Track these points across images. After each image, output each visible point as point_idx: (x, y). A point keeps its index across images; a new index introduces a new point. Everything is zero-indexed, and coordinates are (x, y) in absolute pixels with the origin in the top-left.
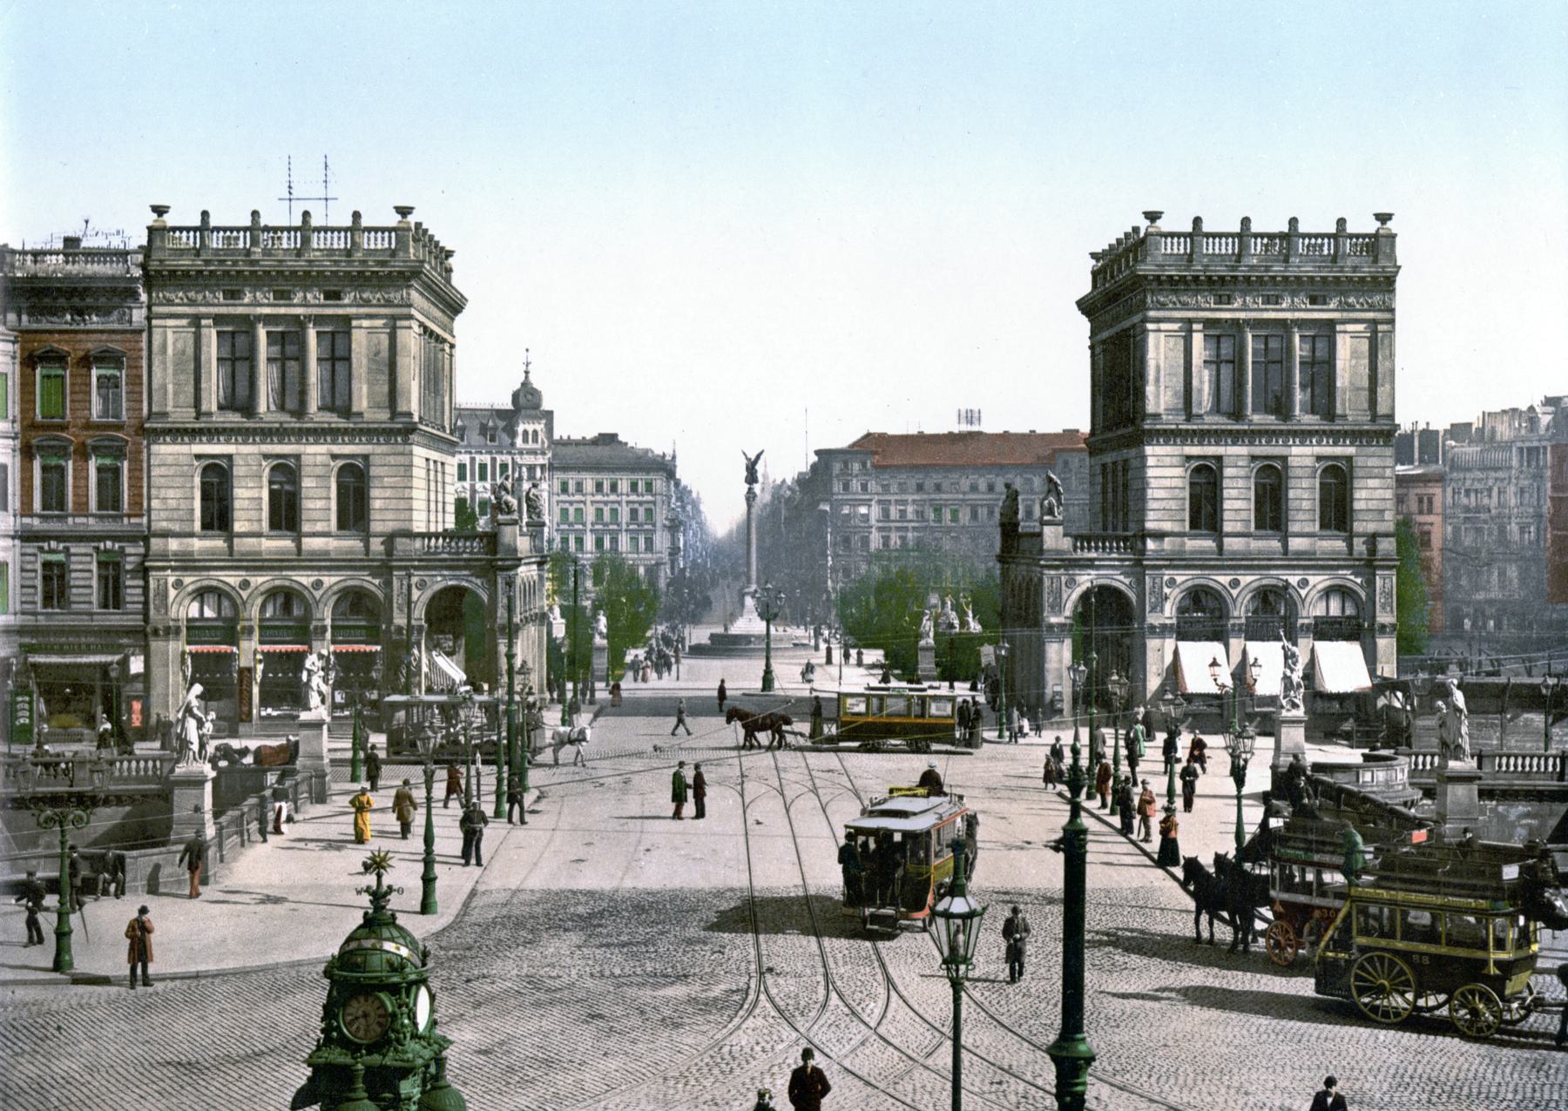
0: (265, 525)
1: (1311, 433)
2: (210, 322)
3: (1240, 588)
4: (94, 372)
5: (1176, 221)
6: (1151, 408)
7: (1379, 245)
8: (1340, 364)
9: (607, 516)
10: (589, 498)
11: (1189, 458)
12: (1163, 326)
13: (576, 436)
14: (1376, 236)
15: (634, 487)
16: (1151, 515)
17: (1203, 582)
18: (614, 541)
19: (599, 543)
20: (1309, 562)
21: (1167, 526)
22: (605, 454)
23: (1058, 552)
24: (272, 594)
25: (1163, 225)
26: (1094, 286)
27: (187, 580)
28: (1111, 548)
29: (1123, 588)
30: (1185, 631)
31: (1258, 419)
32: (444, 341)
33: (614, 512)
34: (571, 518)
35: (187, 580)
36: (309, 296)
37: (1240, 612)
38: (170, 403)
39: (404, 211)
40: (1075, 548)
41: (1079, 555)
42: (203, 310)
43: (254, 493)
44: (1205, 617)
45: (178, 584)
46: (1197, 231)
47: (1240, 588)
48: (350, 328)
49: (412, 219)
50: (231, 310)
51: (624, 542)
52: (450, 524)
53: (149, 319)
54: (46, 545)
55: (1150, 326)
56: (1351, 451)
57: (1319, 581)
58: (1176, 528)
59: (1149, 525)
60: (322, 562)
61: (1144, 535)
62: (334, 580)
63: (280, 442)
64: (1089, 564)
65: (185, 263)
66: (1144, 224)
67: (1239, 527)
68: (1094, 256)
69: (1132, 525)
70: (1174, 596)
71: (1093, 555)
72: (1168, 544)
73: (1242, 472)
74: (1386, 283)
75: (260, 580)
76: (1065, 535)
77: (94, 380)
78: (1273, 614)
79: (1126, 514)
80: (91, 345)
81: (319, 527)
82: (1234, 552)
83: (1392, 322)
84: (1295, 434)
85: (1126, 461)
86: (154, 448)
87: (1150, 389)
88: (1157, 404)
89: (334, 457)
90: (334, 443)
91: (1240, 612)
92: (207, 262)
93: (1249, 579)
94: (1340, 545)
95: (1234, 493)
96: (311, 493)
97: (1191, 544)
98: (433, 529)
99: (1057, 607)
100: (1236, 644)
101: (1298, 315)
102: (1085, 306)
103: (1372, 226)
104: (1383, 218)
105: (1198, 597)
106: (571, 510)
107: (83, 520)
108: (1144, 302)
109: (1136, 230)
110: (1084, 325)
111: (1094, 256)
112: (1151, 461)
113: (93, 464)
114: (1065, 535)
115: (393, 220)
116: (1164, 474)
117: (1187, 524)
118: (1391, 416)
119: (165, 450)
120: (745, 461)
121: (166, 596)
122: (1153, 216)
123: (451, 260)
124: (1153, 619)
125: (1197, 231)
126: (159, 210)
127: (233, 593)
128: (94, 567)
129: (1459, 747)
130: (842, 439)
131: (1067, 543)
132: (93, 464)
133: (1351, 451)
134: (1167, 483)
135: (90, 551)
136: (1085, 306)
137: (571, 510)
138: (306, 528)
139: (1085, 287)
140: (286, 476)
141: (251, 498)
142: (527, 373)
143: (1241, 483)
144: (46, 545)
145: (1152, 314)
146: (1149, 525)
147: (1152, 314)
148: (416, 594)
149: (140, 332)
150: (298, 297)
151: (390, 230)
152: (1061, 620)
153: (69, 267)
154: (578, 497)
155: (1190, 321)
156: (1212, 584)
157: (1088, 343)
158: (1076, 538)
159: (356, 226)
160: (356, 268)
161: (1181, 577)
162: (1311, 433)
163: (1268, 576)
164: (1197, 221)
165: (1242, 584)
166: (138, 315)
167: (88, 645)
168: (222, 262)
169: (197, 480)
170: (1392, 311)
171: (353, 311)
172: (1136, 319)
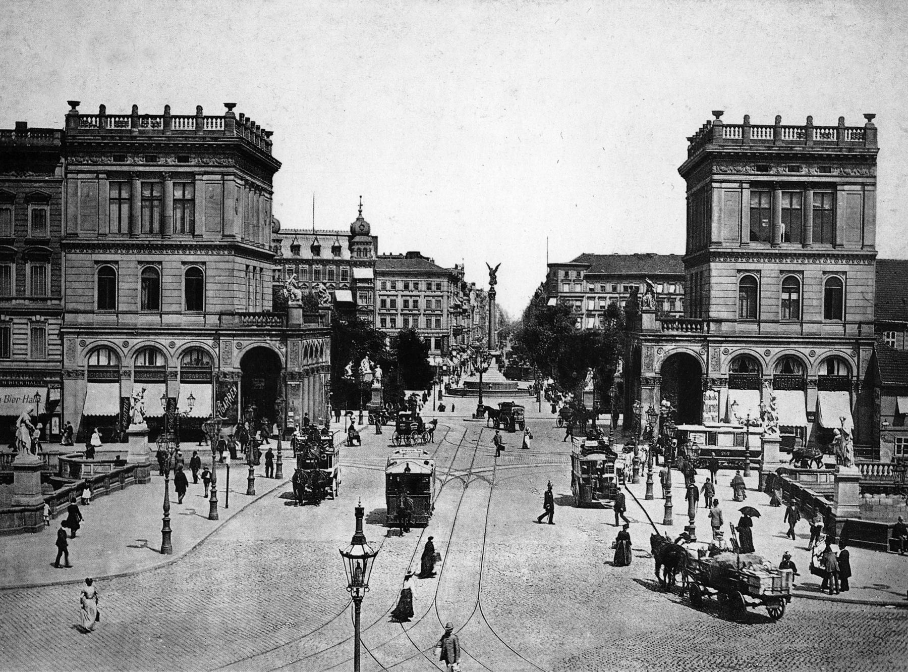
0: (183, 306)
1: (820, 256)
2: (104, 176)
3: (769, 358)
4: (30, 208)
5: (732, 117)
6: (714, 238)
7: (868, 133)
8: (839, 212)
9: (434, 306)
10: (400, 293)
11: (739, 271)
12: (724, 185)
13: (396, 253)
14: (865, 129)
15: (406, 287)
16: (713, 308)
17: (747, 351)
18: (415, 321)
19: (406, 322)
20: (814, 340)
21: (724, 315)
22: (415, 265)
23: (651, 331)
24: (188, 351)
25: (725, 120)
26: (689, 157)
27: (88, 341)
28: (687, 328)
29: (847, 357)
30: (733, 383)
31: (817, 248)
32: (265, 190)
33: (416, 302)
34: (411, 307)
35: (244, 343)
36: (169, 160)
37: (770, 371)
38: (79, 228)
39: (230, 106)
40: (663, 328)
41: (666, 332)
42: (100, 168)
43: (132, 286)
44: (745, 374)
45: (83, 344)
46: (746, 125)
47: (769, 358)
48: (837, 190)
49: (236, 111)
50: (118, 168)
51: (422, 321)
52: (268, 306)
53: (66, 174)
54: (34, 318)
55: (714, 185)
56: (846, 268)
57: (822, 352)
58: (730, 316)
59: (713, 314)
60: (814, 340)
61: (709, 321)
62: (136, 341)
63: (747, 262)
64: (672, 339)
65: (88, 138)
66: (713, 118)
67: (771, 317)
68: (689, 139)
69: (703, 315)
70: (725, 360)
71: (675, 333)
72: (725, 327)
73: (773, 281)
74: (868, 160)
75: (136, 341)
76: (656, 320)
77: (30, 212)
78: (791, 375)
79: (701, 308)
80: (28, 189)
81: (174, 308)
82: (768, 333)
83: (874, 184)
84: (809, 256)
85: (701, 272)
86: (69, 256)
87: (714, 225)
88: (719, 236)
89: (184, 263)
90: (184, 254)
91: (770, 371)
92: (104, 138)
93: (777, 350)
94: (839, 329)
95: (768, 294)
96: (169, 286)
97: (739, 327)
98: (251, 311)
99: (650, 366)
100: (812, 392)
101: (811, 179)
102: (685, 172)
103: (863, 122)
104: (869, 117)
105: (788, 363)
106: (388, 301)
107: (22, 301)
108: (711, 169)
109: (709, 122)
110: (682, 183)
111: (689, 139)
112: (714, 273)
113: (28, 267)
114: (656, 320)
115: (223, 111)
116: (723, 280)
117: (96, 305)
118: (873, 246)
119: (76, 257)
120: (489, 271)
121: (719, 359)
122: (718, 114)
123: (271, 138)
124: (713, 375)
125: (746, 125)
126: (74, 104)
127: (118, 350)
128: (29, 332)
129: (847, 459)
130: (566, 257)
131: (658, 325)
132: (28, 267)
133: (846, 268)
134: (724, 287)
135: (25, 321)
136: (685, 172)
137: (388, 301)
138: (806, 318)
139: (682, 157)
140: (791, 283)
141: (771, 295)
142: (360, 211)
143: (773, 288)
144: (34, 318)
145: (716, 177)
146: (713, 314)
147: (716, 177)
148: (723, 357)
149: (61, 182)
150: (804, 171)
151: (221, 118)
152: (653, 375)
153: (35, 141)
154: (393, 293)
155: (741, 182)
156: (752, 353)
157: (686, 195)
158: (663, 321)
159: (199, 115)
160: (198, 142)
161: (731, 347)
162: (820, 256)
163: (682, 347)
164: (746, 118)
165: (177, 346)
166: (59, 172)
167: (24, 381)
168: (113, 138)
169: (96, 276)
170: (875, 177)
171: (197, 169)
172: (708, 180)
